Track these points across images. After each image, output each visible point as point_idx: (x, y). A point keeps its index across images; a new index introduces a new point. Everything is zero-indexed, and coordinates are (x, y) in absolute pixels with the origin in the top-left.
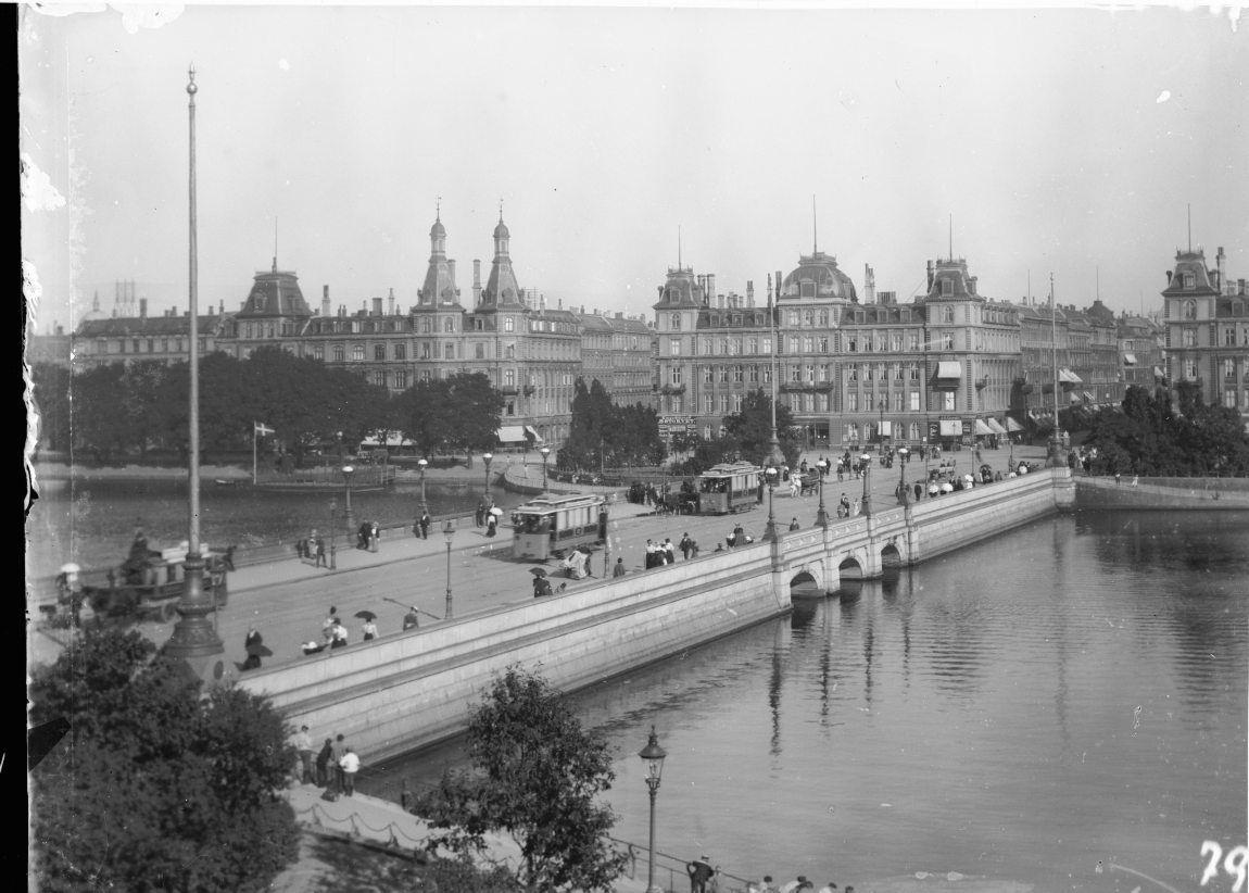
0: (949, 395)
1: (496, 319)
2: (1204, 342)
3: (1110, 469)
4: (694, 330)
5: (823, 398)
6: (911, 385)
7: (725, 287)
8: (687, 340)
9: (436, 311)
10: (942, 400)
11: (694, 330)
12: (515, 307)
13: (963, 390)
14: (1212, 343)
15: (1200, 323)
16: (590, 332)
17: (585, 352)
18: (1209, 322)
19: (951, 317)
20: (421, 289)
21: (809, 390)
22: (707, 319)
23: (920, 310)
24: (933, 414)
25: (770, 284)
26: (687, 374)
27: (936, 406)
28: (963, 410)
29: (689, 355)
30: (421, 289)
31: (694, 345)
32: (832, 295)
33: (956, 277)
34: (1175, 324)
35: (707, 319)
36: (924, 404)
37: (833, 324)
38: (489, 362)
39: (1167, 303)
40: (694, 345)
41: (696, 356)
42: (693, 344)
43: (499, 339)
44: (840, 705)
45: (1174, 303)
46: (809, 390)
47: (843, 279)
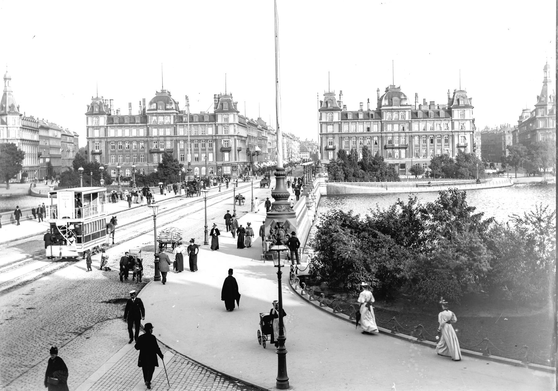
0: (226, 154)
1: (6, 118)
2: (336, 131)
3: (351, 188)
4: (106, 125)
5: (403, 151)
6: (438, 146)
7: (121, 107)
8: (102, 130)
9: (6, 115)
10: (223, 156)
11: (106, 125)
12: (16, 113)
13: (233, 152)
14: (105, 136)
15: (334, 122)
16: (42, 128)
17: (41, 137)
18: (338, 122)
19: (464, 115)
20: (539, 95)
21: (396, 148)
22: (180, 118)
23: (214, 117)
24: (219, 163)
25: (140, 104)
26: (103, 145)
27: (221, 159)
28: (233, 161)
29: (104, 137)
30: (539, 95)
31: (106, 131)
32: (172, 109)
33: (229, 102)
34: (324, 123)
35: (111, 120)
36: (215, 158)
37: (407, 119)
38: (4, 139)
39: (321, 114)
40: (106, 131)
41: (463, 130)
42: (105, 131)
43: (9, 128)
44: (181, 388)
45: (324, 114)
46: (396, 148)
47: (177, 104)
